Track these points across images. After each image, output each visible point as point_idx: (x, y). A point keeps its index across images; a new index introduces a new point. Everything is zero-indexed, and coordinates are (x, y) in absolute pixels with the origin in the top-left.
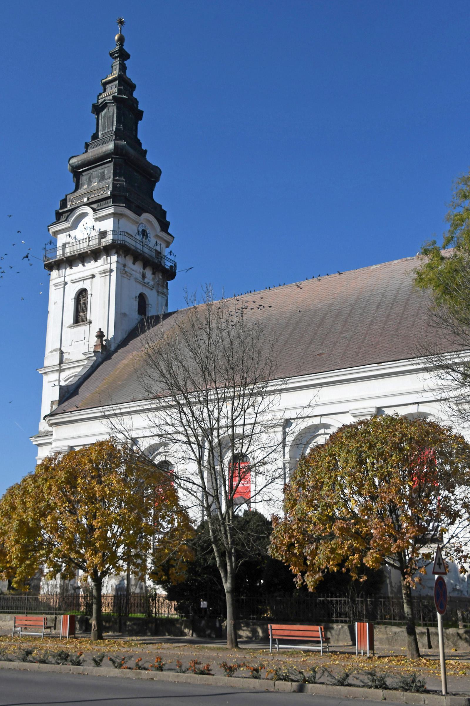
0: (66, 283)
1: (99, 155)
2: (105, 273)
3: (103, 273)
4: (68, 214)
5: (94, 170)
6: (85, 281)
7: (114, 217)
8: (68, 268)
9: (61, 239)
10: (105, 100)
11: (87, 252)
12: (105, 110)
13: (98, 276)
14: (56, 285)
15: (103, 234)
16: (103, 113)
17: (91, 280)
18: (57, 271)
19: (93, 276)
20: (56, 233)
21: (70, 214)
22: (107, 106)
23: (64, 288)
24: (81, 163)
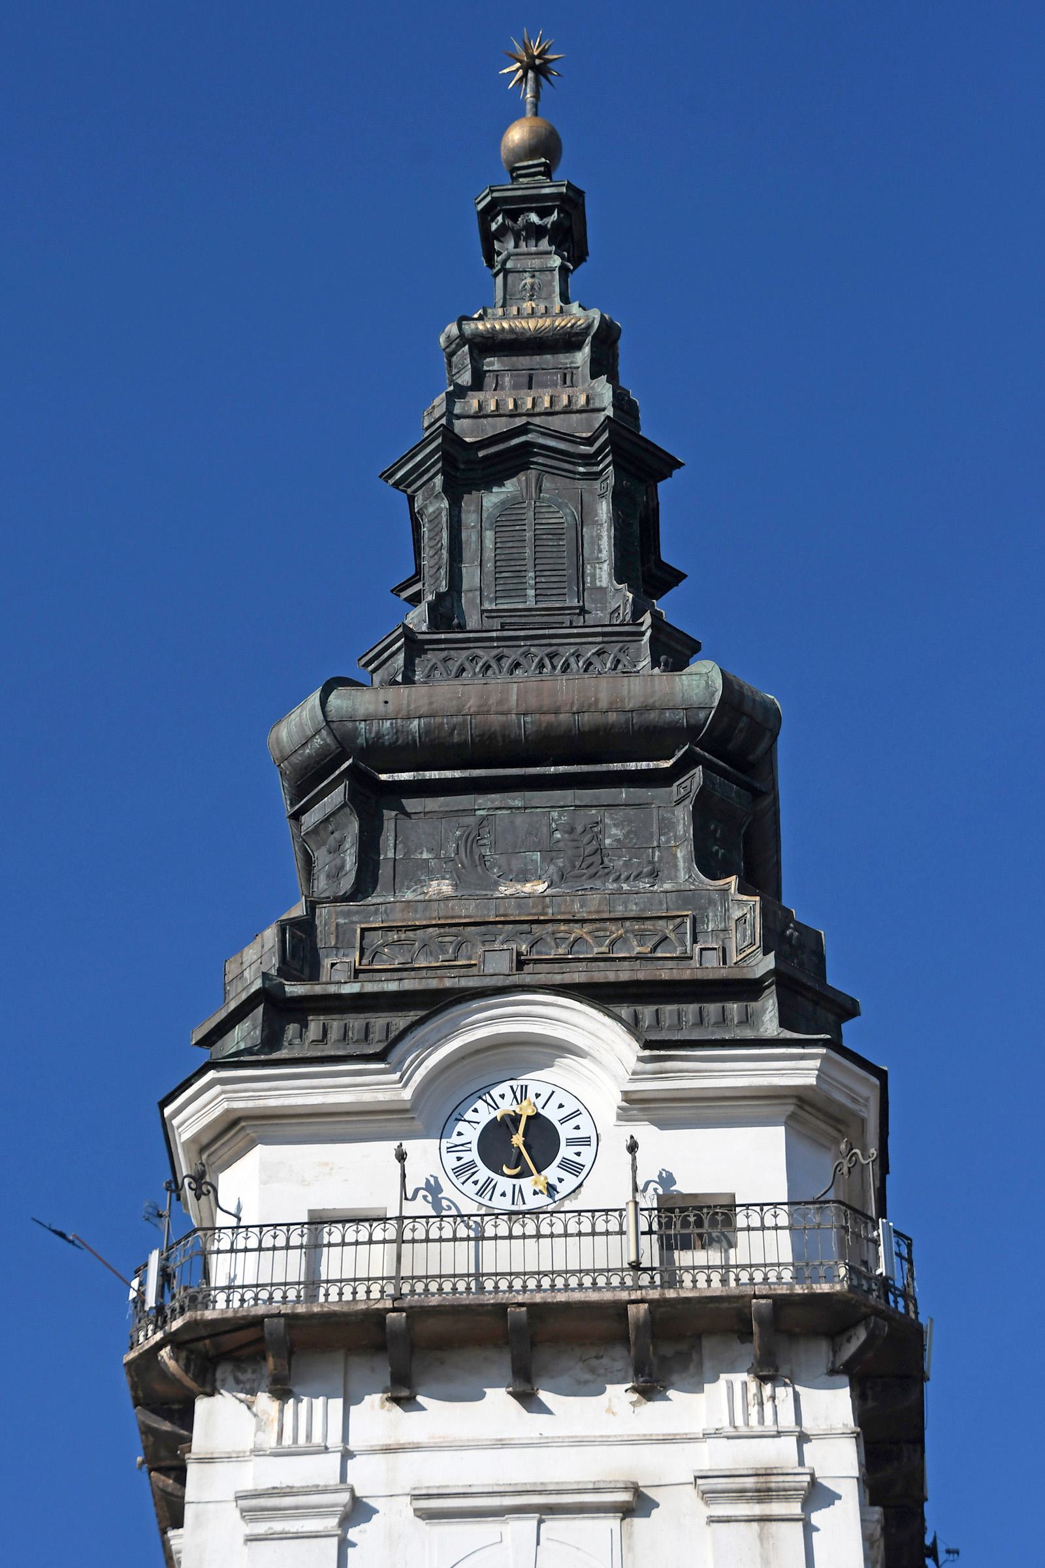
0: (357, 1511)
1: (496, 721)
2: (764, 1494)
3: (740, 1494)
4: (400, 1021)
5: (516, 799)
6: (555, 1527)
7: (793, 1124)
8: (374, 1401)
9: (256, 1186)
10: (523, 430)
11: (619, 1309)
12: (511, 487)
13: (680, 1509)
14: (257, 1506)
15: (693, 1219)
16: (492, 499)
17: (611, 1523)
18: (264, 1401)
19: (637, 1505)
20: (234, 1133)
21: (422, 1021)
22: (525, 467)
23: (344, 1545)
24: (427, 732)
